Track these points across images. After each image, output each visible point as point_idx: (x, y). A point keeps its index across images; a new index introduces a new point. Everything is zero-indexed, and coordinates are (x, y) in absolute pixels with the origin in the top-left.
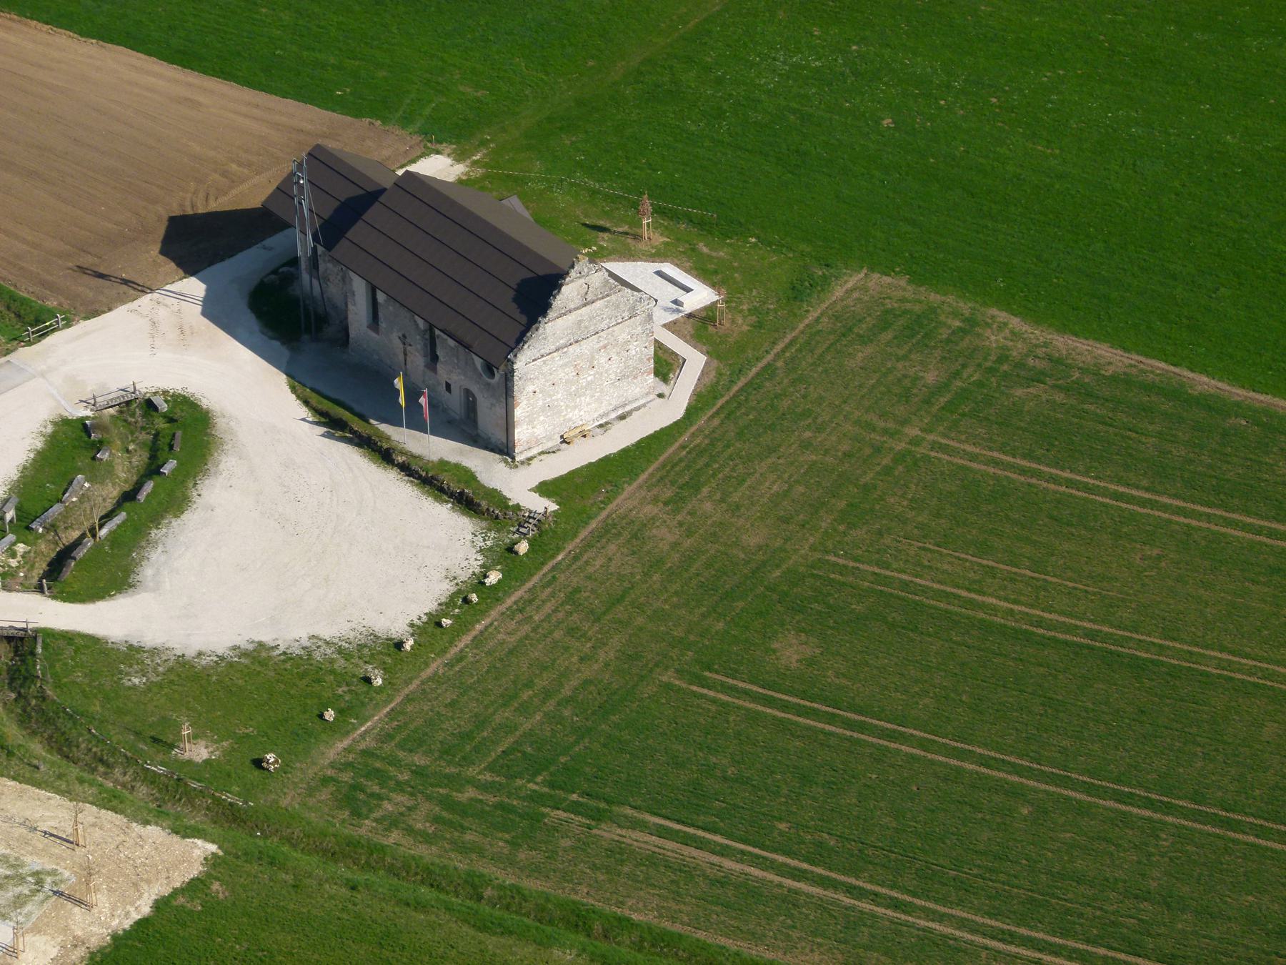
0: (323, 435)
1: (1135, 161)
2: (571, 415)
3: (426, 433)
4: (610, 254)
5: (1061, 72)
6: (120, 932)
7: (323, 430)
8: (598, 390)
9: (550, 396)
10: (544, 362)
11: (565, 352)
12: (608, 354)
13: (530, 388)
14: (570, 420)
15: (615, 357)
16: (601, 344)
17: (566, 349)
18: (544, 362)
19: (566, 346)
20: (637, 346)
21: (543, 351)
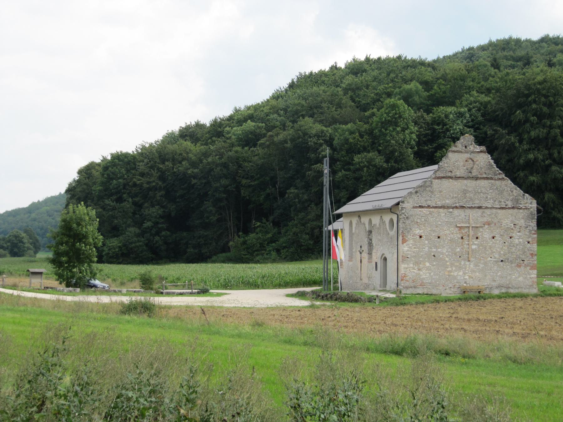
0: (293, 80)
1: (536, 255)
2: (456, 274)
3: (537, 214)
4: (152, 260)
5: (72, 264)
6: (147, 146)
7: (271, 96)
8: (482, 262)
9: (436, 247)
10: (431, 213)
11: (451, 212)
12: (492, 232)
13: (418, 232)
14: (455, 277)
15: (498, 237)
16: (485, 220)
17: (451, 210)
18: (431, 213)
19: (453, 208)
20: (520, 237)
21: (429, 203)
